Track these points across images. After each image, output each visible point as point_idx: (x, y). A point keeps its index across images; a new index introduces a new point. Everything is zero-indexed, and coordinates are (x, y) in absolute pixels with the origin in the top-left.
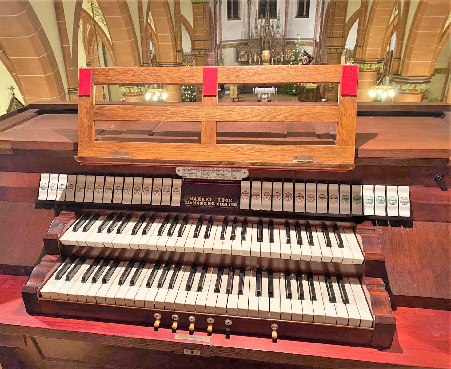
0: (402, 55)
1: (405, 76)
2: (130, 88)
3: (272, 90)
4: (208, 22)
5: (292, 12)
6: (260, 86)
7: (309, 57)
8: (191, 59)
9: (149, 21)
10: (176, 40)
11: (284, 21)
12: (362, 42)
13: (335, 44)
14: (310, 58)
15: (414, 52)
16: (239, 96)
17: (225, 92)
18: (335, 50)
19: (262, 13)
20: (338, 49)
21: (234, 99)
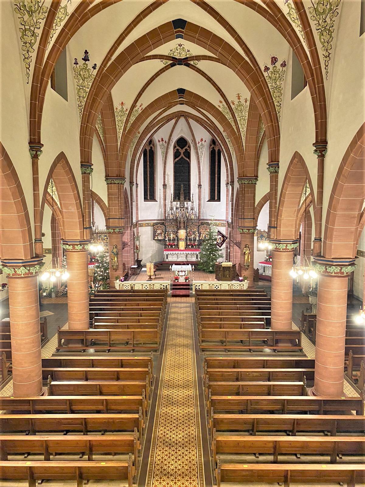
0: (323, 237)
2: (16, 269)
3: (189, 267)
4: (123, 202)
6: (176, 263)
7: (223, 236)
8: (105, 236)
9: (49, 190)
10: (83, 216)
11: (198, 203)
12: (276, 223)
13: (247, 224)
15: (335, 233)
16: (156, 273)
17: (142, 269)
18: (247, 231)
19: (177, 196)
20: (250, 229)
21: (150, 276)
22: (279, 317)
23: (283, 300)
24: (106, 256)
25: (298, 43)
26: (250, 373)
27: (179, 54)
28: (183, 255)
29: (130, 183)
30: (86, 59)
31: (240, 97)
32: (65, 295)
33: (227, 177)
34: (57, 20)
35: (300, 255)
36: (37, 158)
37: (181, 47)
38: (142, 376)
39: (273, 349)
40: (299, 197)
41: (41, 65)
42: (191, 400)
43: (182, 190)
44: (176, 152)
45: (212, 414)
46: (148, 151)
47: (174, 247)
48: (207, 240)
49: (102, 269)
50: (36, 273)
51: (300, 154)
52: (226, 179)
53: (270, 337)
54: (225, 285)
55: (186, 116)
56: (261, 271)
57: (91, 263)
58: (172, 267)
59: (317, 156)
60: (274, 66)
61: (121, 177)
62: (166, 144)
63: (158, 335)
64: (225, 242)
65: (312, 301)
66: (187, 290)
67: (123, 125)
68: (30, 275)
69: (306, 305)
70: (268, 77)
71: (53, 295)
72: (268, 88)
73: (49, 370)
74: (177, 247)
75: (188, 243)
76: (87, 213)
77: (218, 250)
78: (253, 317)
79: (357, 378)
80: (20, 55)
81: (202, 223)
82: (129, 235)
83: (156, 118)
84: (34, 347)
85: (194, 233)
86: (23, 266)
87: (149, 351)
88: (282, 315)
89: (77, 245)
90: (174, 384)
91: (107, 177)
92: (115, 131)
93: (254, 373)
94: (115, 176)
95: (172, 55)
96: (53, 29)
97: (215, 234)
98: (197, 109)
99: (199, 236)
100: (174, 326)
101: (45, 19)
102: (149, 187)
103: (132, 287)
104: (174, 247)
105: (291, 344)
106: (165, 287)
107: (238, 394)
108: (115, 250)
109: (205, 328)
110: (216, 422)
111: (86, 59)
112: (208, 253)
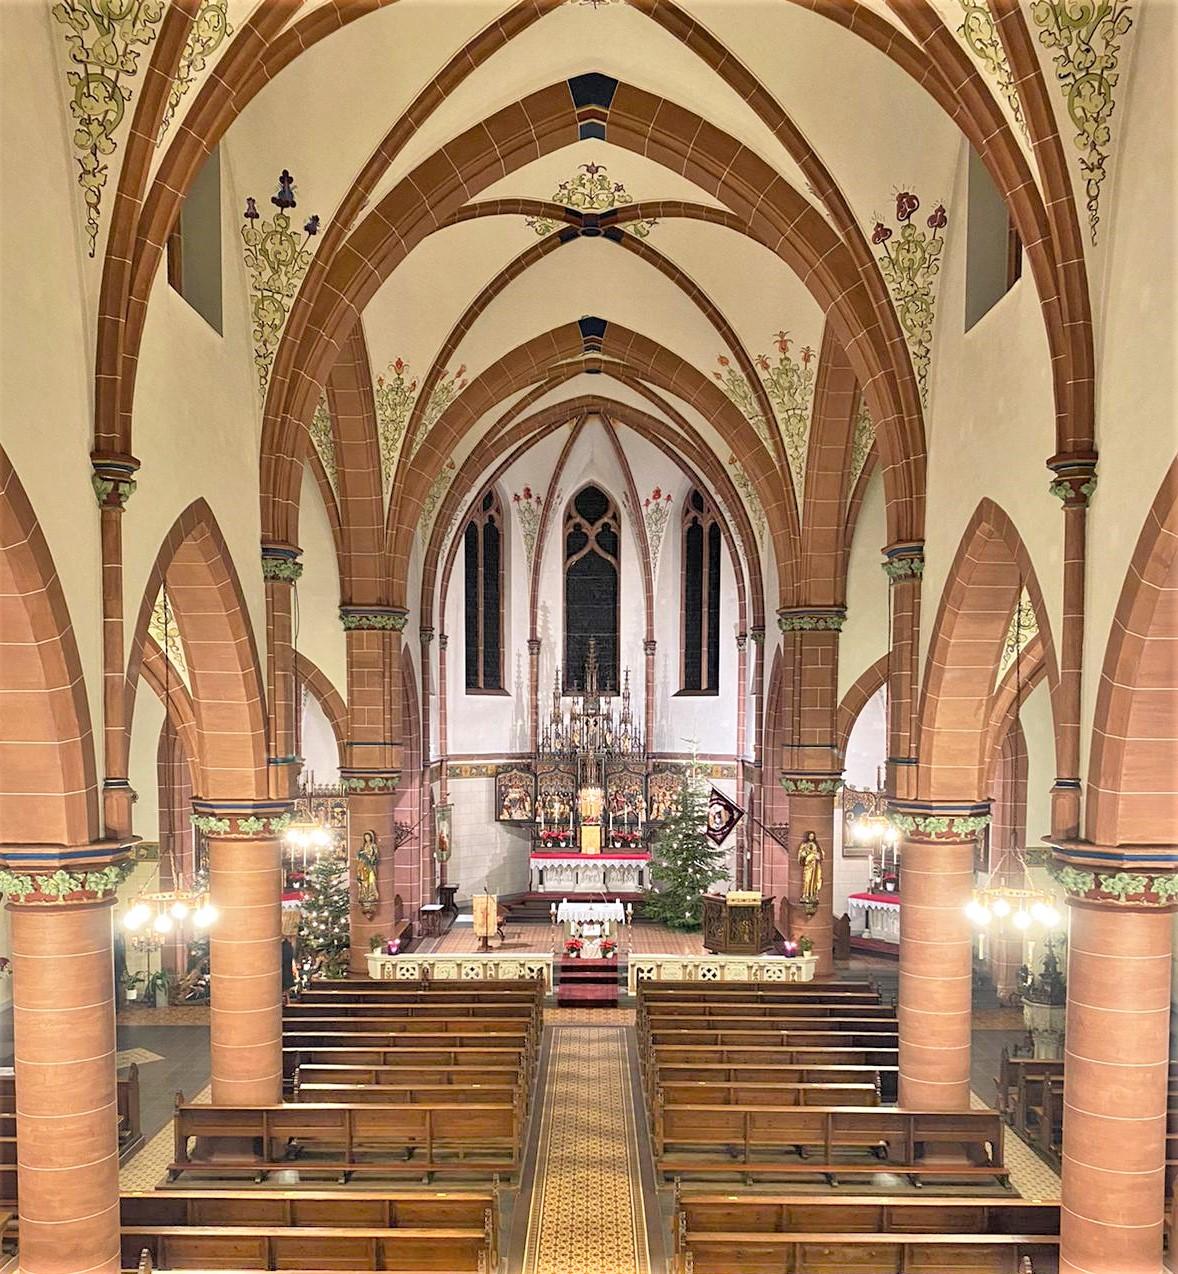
2: (39, 879)
3: (616, 910)
4: (397, 688)
5: (665, 677)
6: (573, 897)
7: (729, 807)
10: (267, 721)
11: (644, 703)
13: (809, 765)
15: (1127, 759)
18: (812, 786)
19: (574, 679)
20: (822, 780)
21: (485, 939)
24: (341, 871)
25: (995, 126)
26: (832, 1249)
27: (588, 199)
28: (595, 872)
30: (285, 200)
32: (202, 997)
33: (743, 615)
34: (191, 48)
35: (986, 871)
36: (120, 504)
37: (596, 176)
41: (136, 192)
43: (592, 660)
46: (481, 530)
47: (563, 845)
48: (677, 822)
49: (326, 914)
50: (106, 893)
51: (997, 506)
52: (738, 621)
53: (896, 1134)
54: (736, 968)
55: (606, 411)
56: (856, 926)
57: (289, 893)
58: (557, 908)
59: (1063, 503)
60: (906, 222)
63: (516, 1127)
64: (734, 830)
65: (1033, 1019)
66: (610, 986)
67: (400, 435)
68: (85, 901)
69: (1027, 1029)
70: (887, 260)
71: (162, 999)
74: (575, 845)
75: (612, 834)
76: (281, 712)
77: (710, 855)
78: (840, 1073)
80: (68, 162)
81: (658, 766)
84: (94, 1151)
85: (631, 799)
88: (938, 1058)
89: (246, 817)
91: (347, 606)
92: (375, 451)
94: (375, 601)
95: (565, 201)
96: (179, 79)
97: (702, 801)
99: (649, 811)
100: (566, 1100)
101: (153, 43)
102: (481, 648)
103: (425, 972)
104: (563, 845)
105: (969, 1157)
106: (534, 975)
108: (369, 849)
109: (675, 1102)
111: (285, 200)
112: (679, 863)
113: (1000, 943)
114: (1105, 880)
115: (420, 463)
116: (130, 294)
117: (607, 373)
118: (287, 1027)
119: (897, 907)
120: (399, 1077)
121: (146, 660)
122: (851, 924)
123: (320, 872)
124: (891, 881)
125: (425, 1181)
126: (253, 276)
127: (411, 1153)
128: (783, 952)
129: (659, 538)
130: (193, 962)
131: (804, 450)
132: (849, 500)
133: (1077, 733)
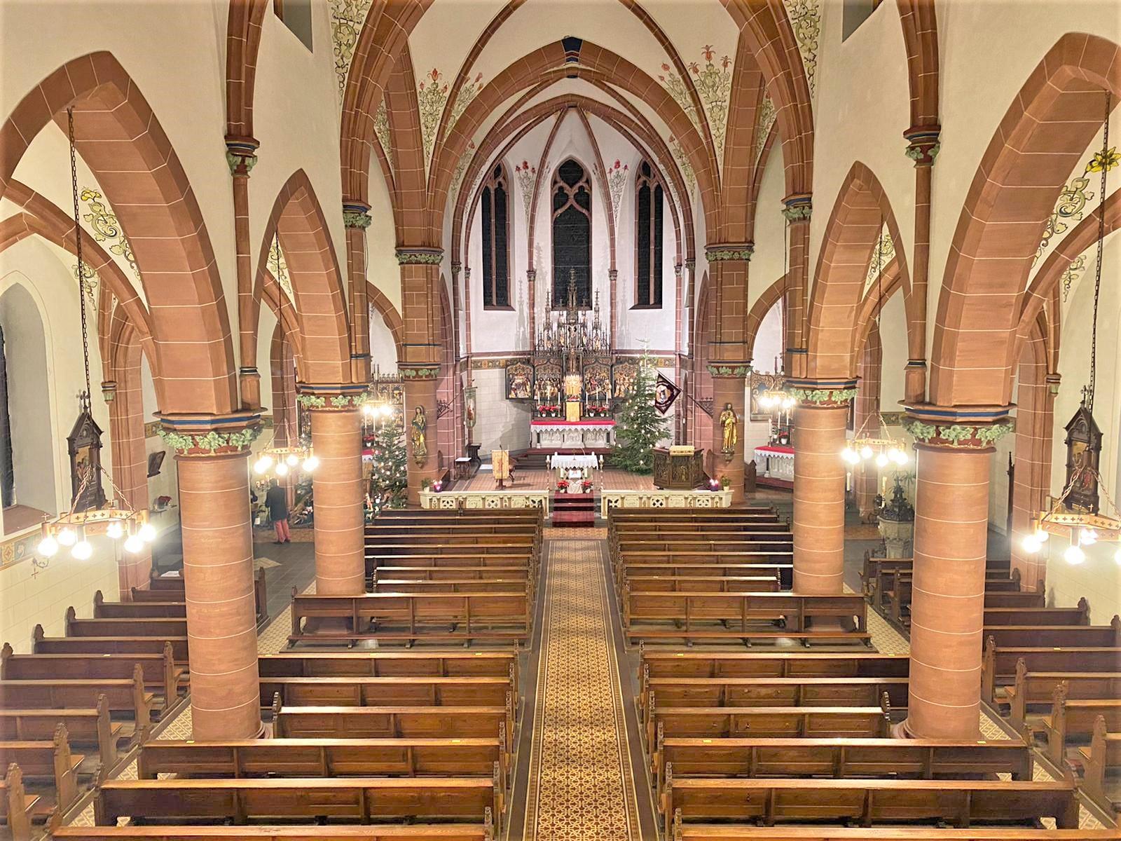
1: (946, 405)
2: (197, 438)
3: (592, 460)
6: (560, 452)
7: (670, 387)
8: (397, 389)
9: (269, 266)
10: (349, 328)
11: (609, 314)
13: (728, 356)
14: (672, 390)
16: (514, 474)
17: (479, 466)
18: (730, 371)
19: (560, 297)
21: (501, 481)
22: (813, 565)
23: (821, 524)
24: (400, 434)
26: (750, 688)
28: (576, 434)
29: (453, 264)
31: (712, 54)
35: (852, 429)
36: (246, 172)
38: (497, 695)
39: (800, 638)
40: (861, 276)
42: (612, 752)
43: (572, 285)
44: (556, 194)
45: (669, 779)
46: (492, 192)
47: (553, 415)
48: (633, 398)
49: (390, 464)
50: (244, 447)
51: (866, 166)
52: (675, 255)
53: (792, 611)
54: (677, 499)
56: (760, 469)
57: (364, 449)
59: (915, 163)
61: (433, 247)
62: (536, 175)
64: (674, 403)
65: (886, 531)
66: (589, 512)
67: (436, 124)
72: (786, 16)
73: (276, 682)
75: (588, 407)
76: (359, 322)
77: (657, 421)
79: (1008, 701)
81: (620, 359)
82: (451, 385)
83: (512, 111)
84: (241, 625)
86: (215, 430)
87: (505, 645)
89: (336, 396)
90: (568, 717)
91: (400, 247)
93: (759, 689)
97: (651, 383)
98: (609, 87)
99: (613, 390)
100: (562, 589)
102: (494, 277)
103: (461, 504)
104: (553, 415)
105: (843, 626)
106: (536, 505)
107: (725, 735)
108: (419, 419)
109: (637, 590)
110: (679, 798)
112: (635, 426)
113: (861, 479)
114: (944, 430)
115: (449, 145)
116: (249, 21)
117: (582, 78)
118: (367, 542)
119: (793, 456)
120: (445, 575)
121: (259, 290)
122: (756, 467)
123: (385, 435)
124: (785, 437)
125: (466, 645)
126: (332, 8)
127: (454, 627)
128: (709, 487)
129: (619, 196)
130: (299, 498)
131: (723, 131)
132: (756, 167)
133: (924, 327)
